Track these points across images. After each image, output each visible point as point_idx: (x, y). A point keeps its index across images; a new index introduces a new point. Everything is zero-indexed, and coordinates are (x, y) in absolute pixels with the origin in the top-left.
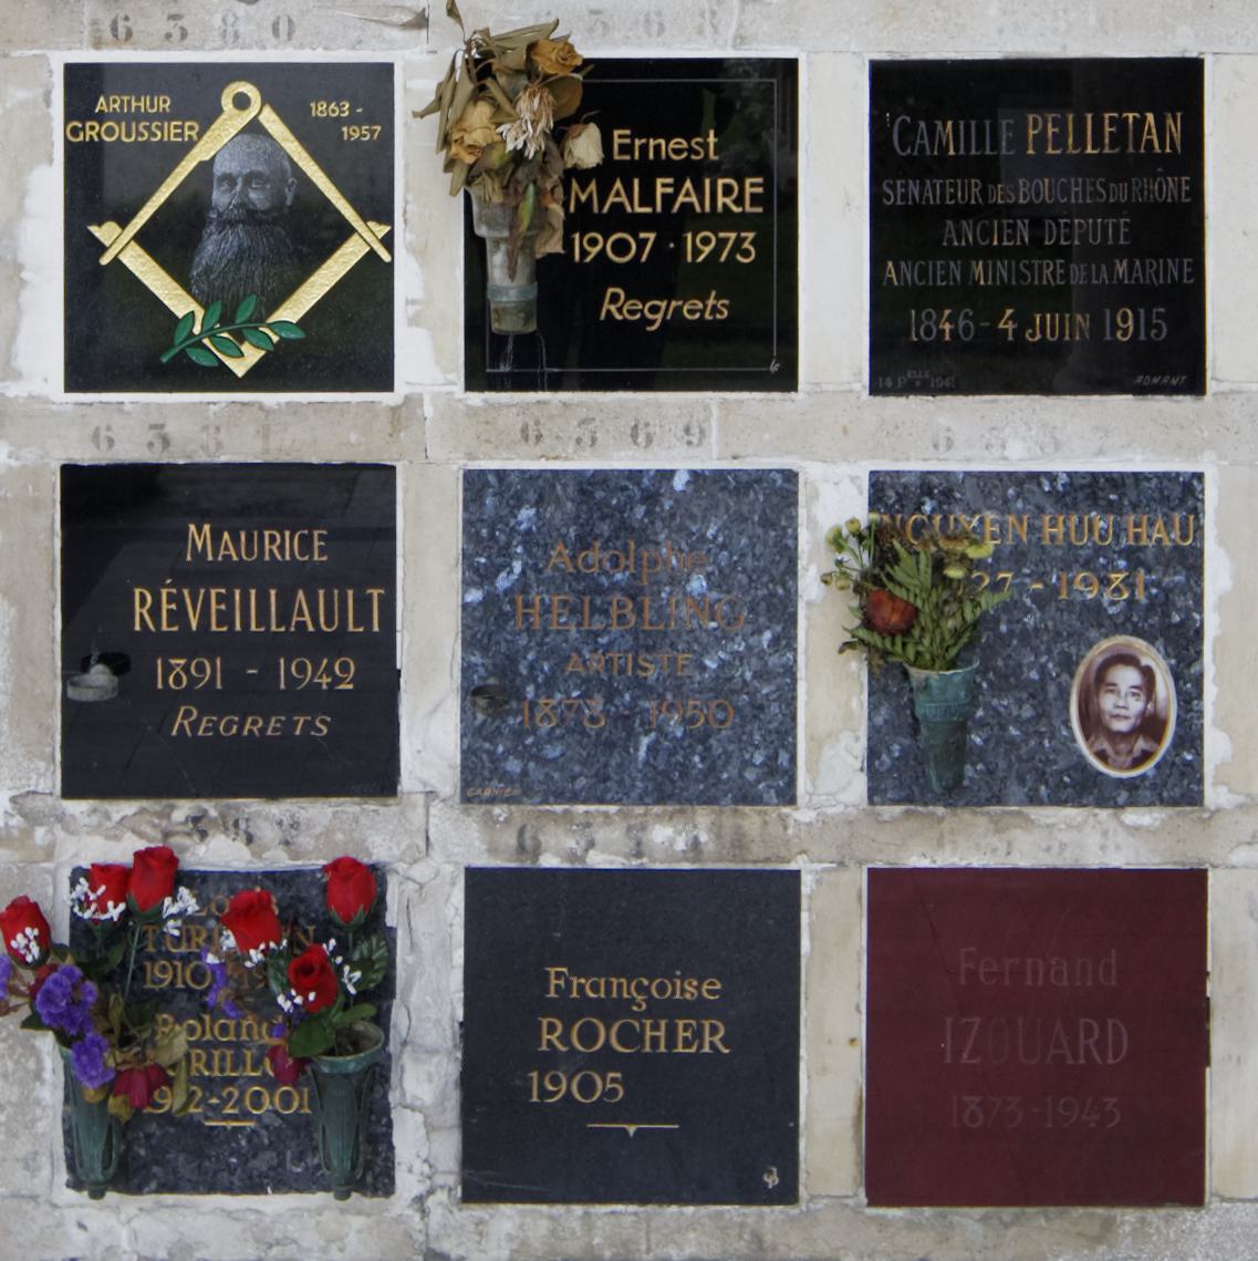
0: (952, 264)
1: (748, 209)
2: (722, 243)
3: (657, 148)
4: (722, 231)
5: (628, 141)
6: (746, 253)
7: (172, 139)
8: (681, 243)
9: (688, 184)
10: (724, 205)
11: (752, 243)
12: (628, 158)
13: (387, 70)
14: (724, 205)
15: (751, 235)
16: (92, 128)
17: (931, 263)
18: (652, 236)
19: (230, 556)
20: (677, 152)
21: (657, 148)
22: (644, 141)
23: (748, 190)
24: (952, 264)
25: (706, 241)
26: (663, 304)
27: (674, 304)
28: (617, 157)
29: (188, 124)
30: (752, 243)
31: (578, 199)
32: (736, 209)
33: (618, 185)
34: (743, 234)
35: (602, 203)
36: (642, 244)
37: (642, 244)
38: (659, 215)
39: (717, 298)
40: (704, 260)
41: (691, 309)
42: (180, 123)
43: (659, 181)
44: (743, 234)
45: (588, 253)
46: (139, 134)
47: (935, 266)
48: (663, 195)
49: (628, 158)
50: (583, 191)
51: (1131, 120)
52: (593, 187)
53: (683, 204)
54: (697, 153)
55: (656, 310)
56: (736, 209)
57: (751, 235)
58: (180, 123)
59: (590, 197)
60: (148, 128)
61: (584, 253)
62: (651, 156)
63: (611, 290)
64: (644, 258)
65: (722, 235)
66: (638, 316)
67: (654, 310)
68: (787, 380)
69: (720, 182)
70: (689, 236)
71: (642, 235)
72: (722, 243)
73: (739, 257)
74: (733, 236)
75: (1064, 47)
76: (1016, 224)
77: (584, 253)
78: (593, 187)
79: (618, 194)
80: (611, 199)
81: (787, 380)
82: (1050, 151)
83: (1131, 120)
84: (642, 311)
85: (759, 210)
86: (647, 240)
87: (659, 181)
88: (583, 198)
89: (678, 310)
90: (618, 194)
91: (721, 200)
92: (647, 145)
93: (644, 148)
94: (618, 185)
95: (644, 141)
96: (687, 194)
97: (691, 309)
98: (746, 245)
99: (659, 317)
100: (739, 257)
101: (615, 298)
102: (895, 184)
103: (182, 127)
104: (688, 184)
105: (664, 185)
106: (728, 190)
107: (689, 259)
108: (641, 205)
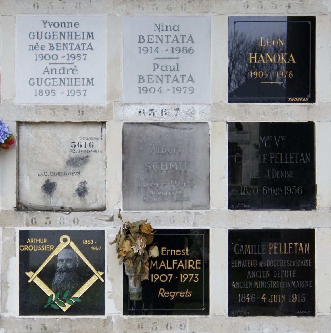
0: (250, 282)
1: (197, 268)
2: (190, 277)
3: (173, 252)
4: (190, 274)
5: (165, 250)
6: (196, 280)
7: (47, 250)
8: (179, 277)
9: (181, 262)
10: (190, 267)
11: (198, 277)
12: (165, 255)
13: (103, 232)
14: (190, 267)
15: (197, 275)
16: (26, 247)
17: (244, 282)
18: (172, 275)
19: (292, 61)
20: (178, 253)
21: (173, 252)
22: (169, 250)
23: (197, 263)
24: (250, 282)
25: (186, 276)
26: (175, 293)
27: (177, 293)
28: (162, 254)
29: (51, 246)
30: (198, 277)
31: (152, 265)
32: (193, 268)
33: (163, 262)
34: (195, 275)
35: (159, 266)
36: (169, 277)
37: (169, 277)
38: (173, 269)
39: (189, 291)
40: (185, 281)
41: (182, 294)
42: (49, 246)
43: (174, 261)
44: (195, 275)
45: (155, 280)
46: (38, 249)
47: (245, 283)
48: (175, 264)
49: (165, 255)
50: (154, 263)
51: (296, 245)
52: (156, 262)
53: (180, 267)
54: (183, 254)
55: (173, 294)
56: (193, 268)
57: (197, 275)
58: (49, 246)
59: (155, 265)
60: (41, 247)
61: (154, 279)
62: (171, 254)
63: (161, 289)
64: (170, 281)
65: (190, 275)
66: (168, 296)
67: (172, 294)
68: (207, 312)
69: (189, 261)
70: (181, 275)
71: (169, 275)
72: (190, 277)
73: (194, 281)
74: (193, 275)
75: (279, 226)
76: (266, 272)
77: (154, 279)
78: (156, 262)
79: (163, 264)
80: (161, 265)
81: (207, 312)
82: (275, 253)
83: (296, 245)
84: (169, 294)
85: (49, 250)
86: (170, 276)
87: (174, 261)
88: (154, 265)
89: (178, 294)
90: (163, 264)
91: (189, 266)
92: (170, 251)
93: (170, 252)
94: (163, 262)
95: (169, 250)
96: (181, 264)
97: (182, 294)
98: (196, 277)
99: (173, 296)
100: (194, 281)
101: (162, 291)
102: (235, 262)
103: (50, 247)
104: (181, 262)
105: (175, 262)
106: (191, 263)
107: (181, 281)
108: (169, 267)
